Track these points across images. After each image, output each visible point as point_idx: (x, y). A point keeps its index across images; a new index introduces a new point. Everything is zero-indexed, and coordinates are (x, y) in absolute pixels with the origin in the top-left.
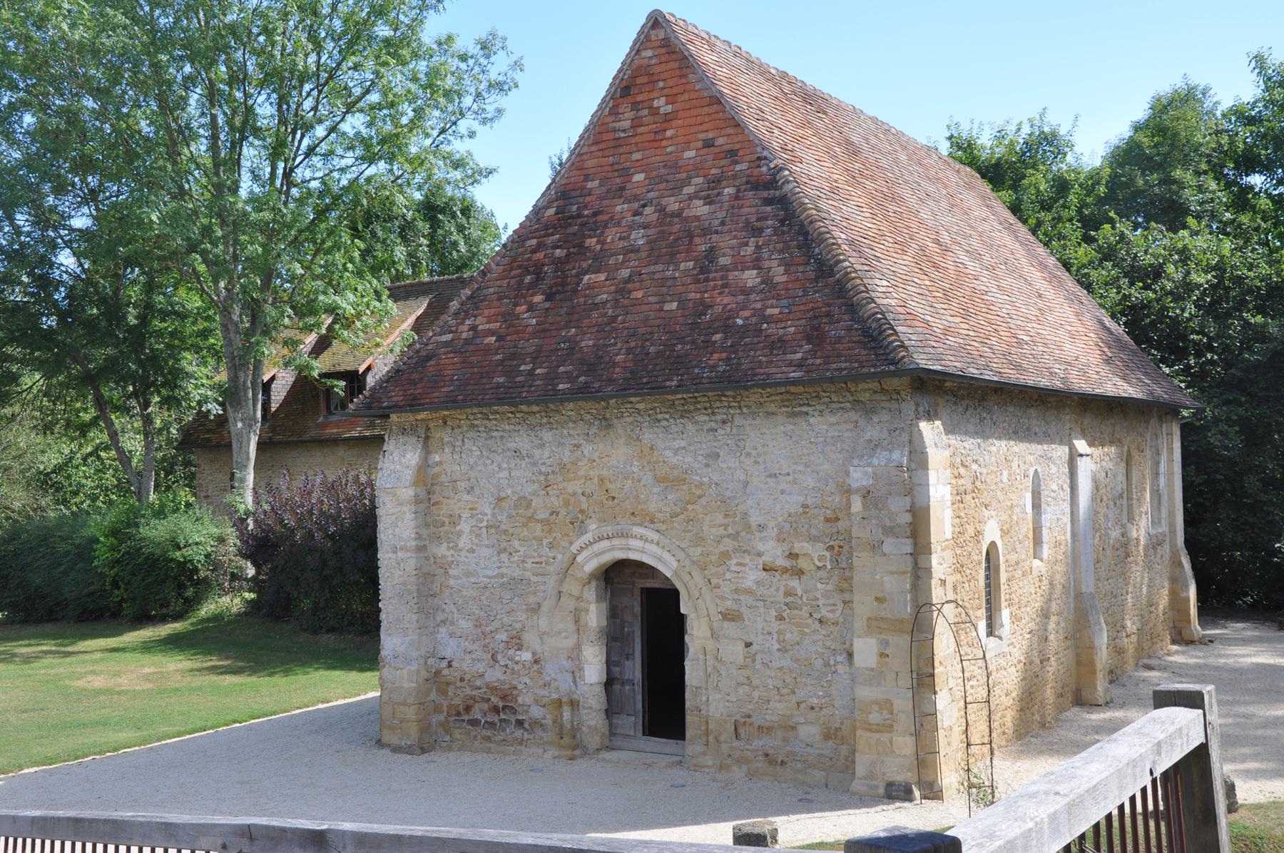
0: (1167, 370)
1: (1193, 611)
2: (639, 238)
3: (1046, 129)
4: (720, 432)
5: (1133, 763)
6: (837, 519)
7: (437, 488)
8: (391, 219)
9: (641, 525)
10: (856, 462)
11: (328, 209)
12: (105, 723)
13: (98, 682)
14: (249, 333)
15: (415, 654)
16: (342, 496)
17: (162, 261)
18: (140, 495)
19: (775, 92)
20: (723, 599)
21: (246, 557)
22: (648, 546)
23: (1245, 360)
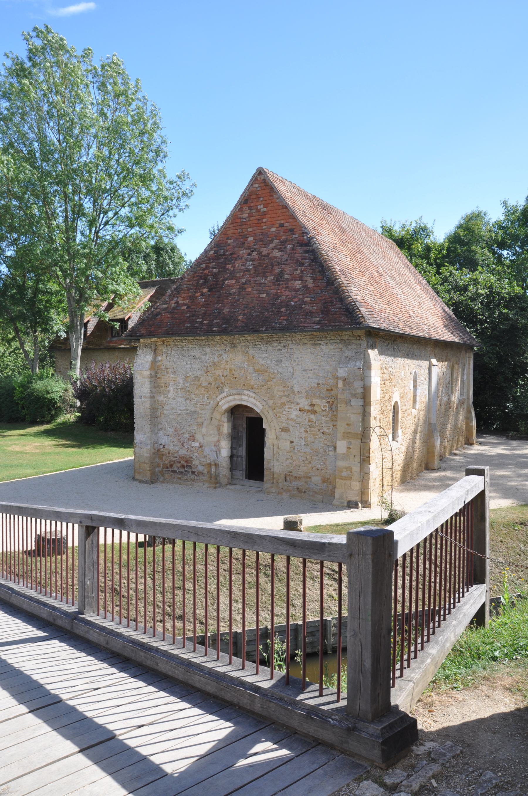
0: (468, 330)
1: (475, 431)
2: (250, 265)
3: (422, 225)
4: (283, 351)
5: (458, 499)
6: (332, 390)
7: (160, 371)
8: (139, 253)
9: (247, 390)
10: (341, 366)
11: (114, 248)
12: (20, 466)
13: (17, 449)
14: (78, 301)
15: (149, 442)
16: (117, 373)
17: (43, 271)
18: (33, 369)
19: (310, 204)
20: (282, 422)
21: (77, 398)
22: (250, 399)
23: (500, 328)
